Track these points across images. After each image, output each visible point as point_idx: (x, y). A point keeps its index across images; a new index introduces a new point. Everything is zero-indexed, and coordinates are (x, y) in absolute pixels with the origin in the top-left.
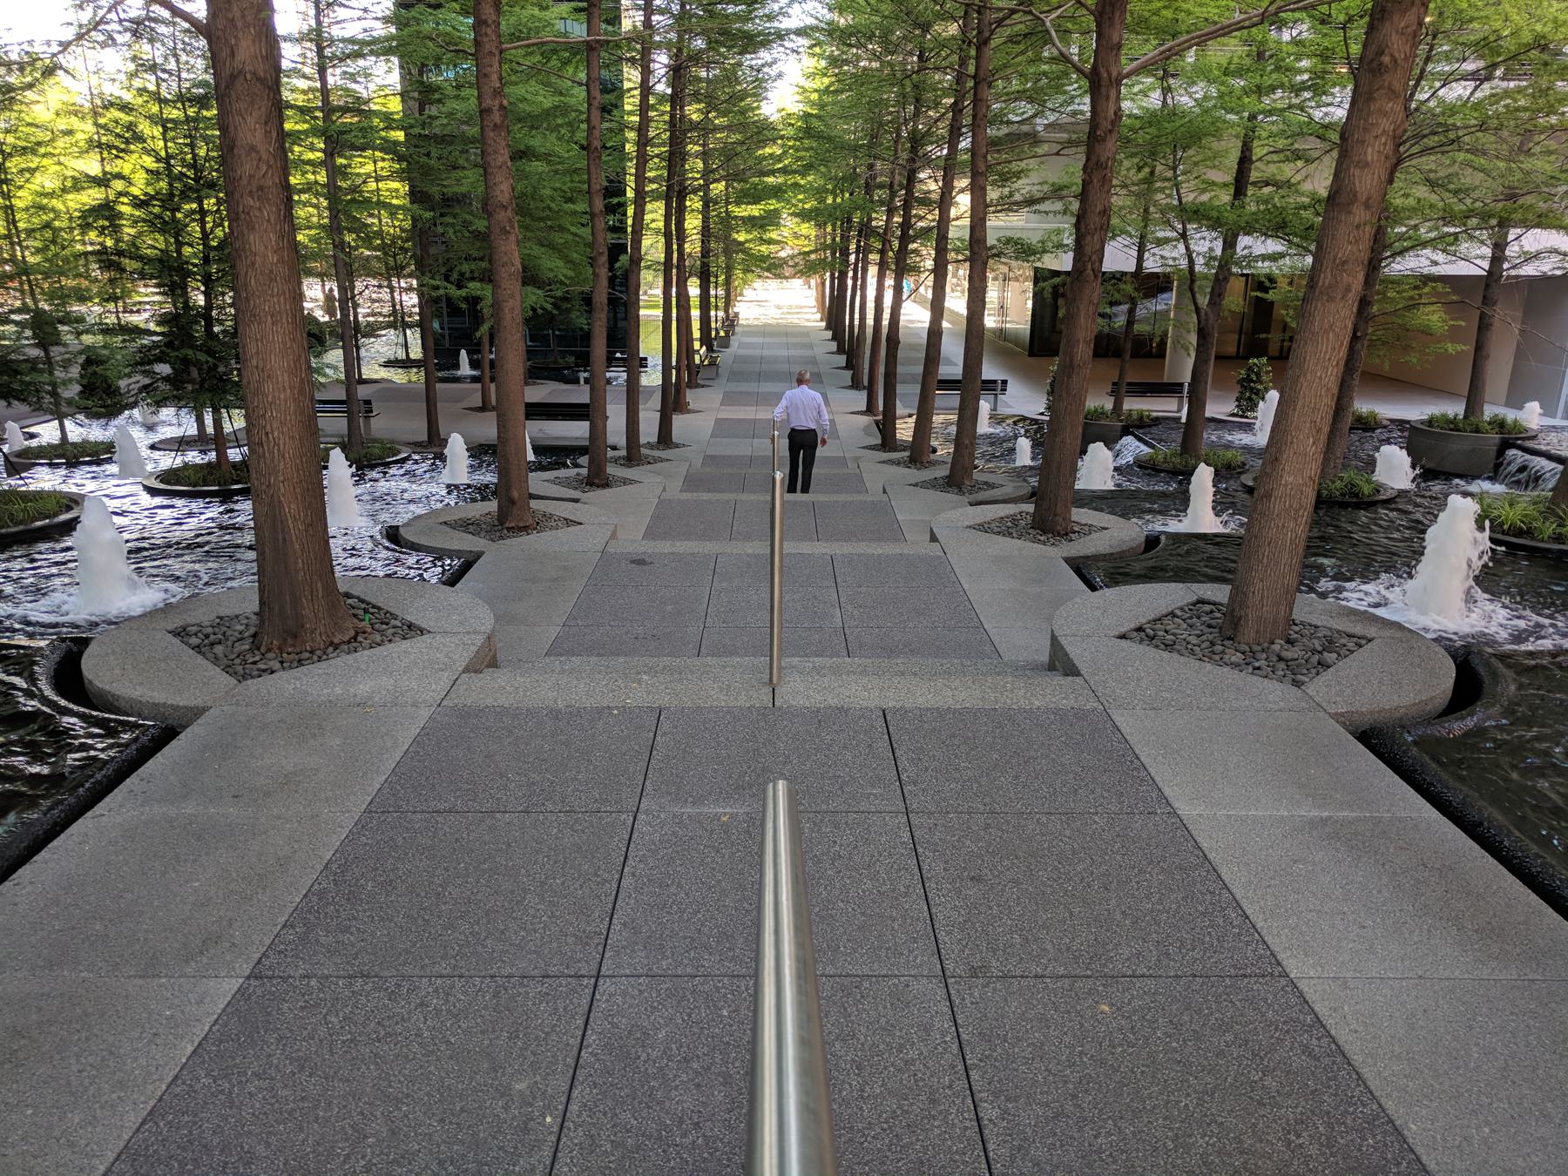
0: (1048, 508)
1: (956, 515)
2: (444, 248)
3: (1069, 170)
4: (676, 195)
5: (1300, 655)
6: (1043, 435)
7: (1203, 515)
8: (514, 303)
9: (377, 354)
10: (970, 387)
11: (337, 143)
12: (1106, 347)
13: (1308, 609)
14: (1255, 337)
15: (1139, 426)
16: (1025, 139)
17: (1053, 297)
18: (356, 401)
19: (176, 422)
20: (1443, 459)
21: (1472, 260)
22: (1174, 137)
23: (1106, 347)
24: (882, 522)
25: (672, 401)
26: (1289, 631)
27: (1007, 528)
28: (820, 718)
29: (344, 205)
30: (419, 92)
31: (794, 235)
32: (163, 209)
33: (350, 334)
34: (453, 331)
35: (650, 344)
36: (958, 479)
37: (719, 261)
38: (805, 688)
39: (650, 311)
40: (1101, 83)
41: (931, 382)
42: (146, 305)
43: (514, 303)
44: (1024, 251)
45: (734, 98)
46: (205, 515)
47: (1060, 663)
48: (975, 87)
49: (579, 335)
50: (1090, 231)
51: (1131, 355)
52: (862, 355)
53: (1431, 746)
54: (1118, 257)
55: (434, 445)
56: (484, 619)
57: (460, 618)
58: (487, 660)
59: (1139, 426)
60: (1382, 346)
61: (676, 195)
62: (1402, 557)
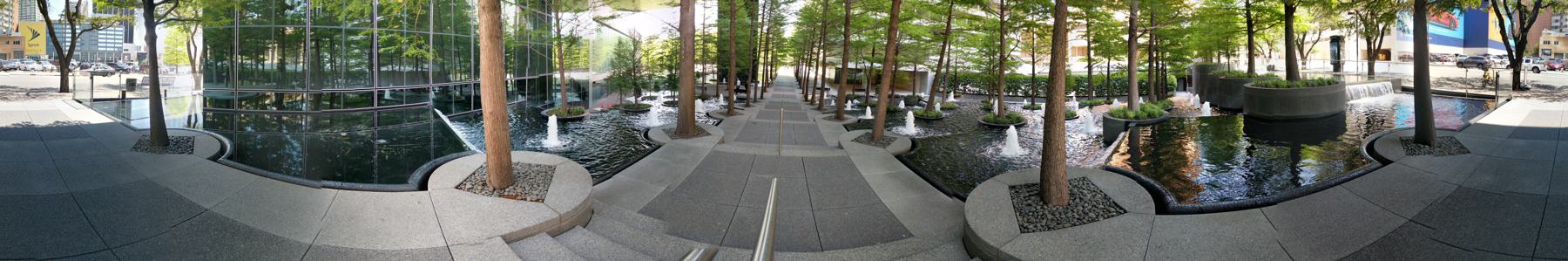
0: (839, 115)
1: (819, 116)
2: (722, 60)
3: (841, 50)
4: (767, 51)
5: (885, 142)
6: (837, 99)
7: (869, 115)
8: (734, 71)
9: (709, 78)
10: (823, 89)
11: (705, 41)
12: (849, 82)
13: (886, 133)
14: (877, 80)
15: (858, 97)
16: (834, 43)
17: (839, 73)
18: (704, 87)
19: (668, 93)
20: (910, 102)
21: (911, 69)
22: (860, 45)
23: (849, 82)
24: (804, 117)
25: (764, 90)
26: (883, 138)
27: (830, 119)
28: (788, 159)
29: (705, 51)
30: (720, 32)
31: (789, 59)
32: (670, 58)
33: (704, 74)
34: (723, 74)
35: (760, 79)
36: (820, 108)
37: (775, 63)
38: (787, 152)
39: (760, 72)
40: (846, 36)
41: (815, 88)
42: (666, 73)
43: (734, 71)
44: (832, 64)
45: (779, 34)
46: (670, 109)
47: (840, 147)
48: (824, 34)
49: (748, 75)
50: (845, 62)
51: (855, 84)
52: (801, 81)
53: (911, 157)
54: (851, 65)
55: (717, 96)
56: (722, 133)
57: (718, 133)
58: (722, 142)
59: (858, 97)
60: (897, 81)
61: (767, 51)
62: (903, 123)
